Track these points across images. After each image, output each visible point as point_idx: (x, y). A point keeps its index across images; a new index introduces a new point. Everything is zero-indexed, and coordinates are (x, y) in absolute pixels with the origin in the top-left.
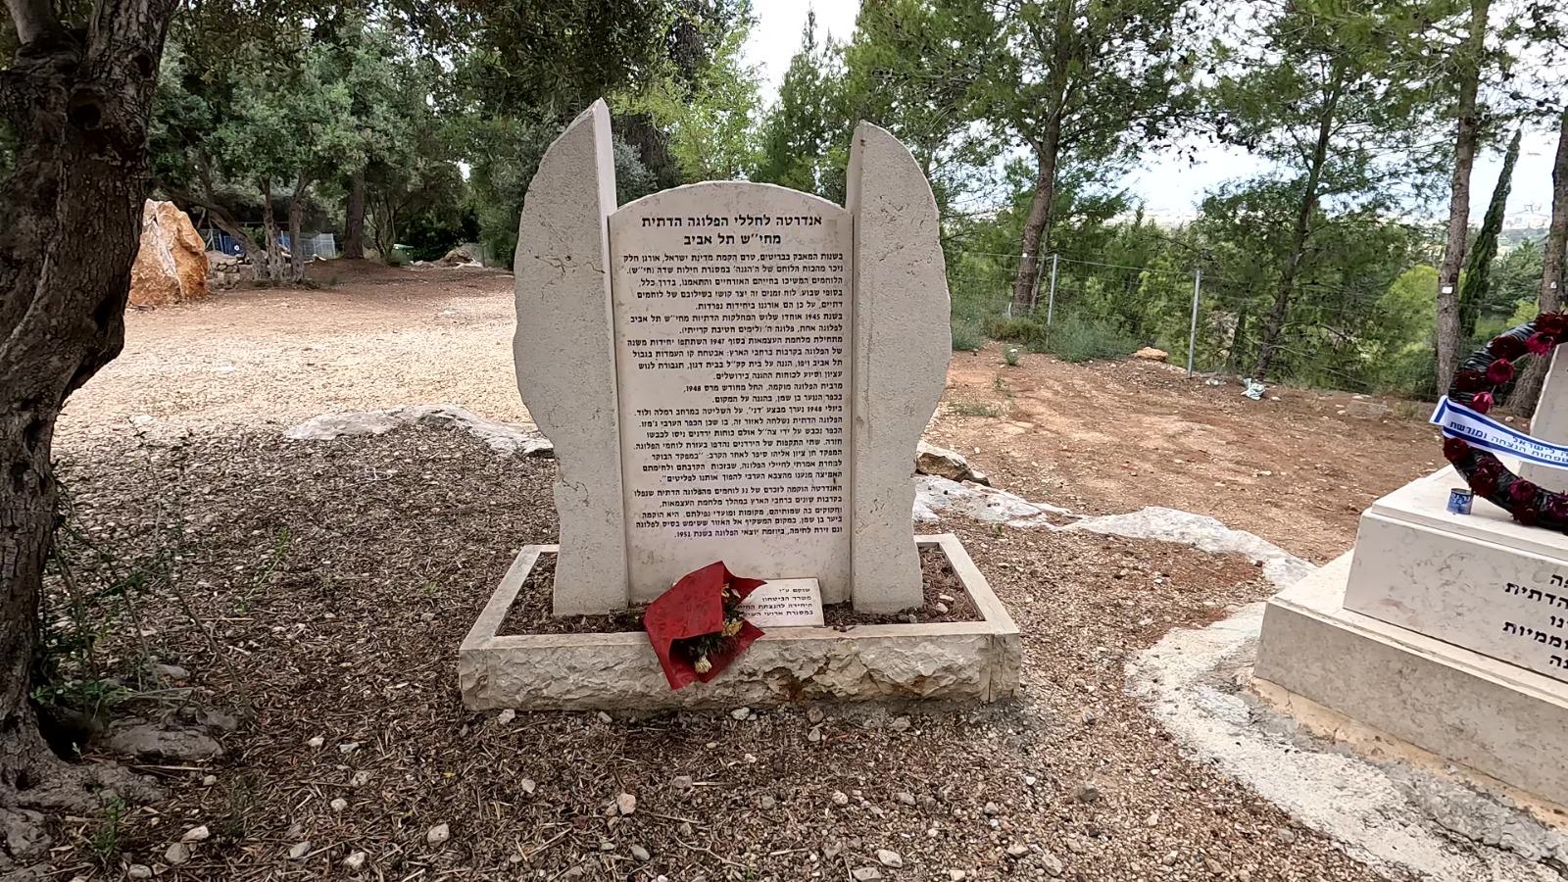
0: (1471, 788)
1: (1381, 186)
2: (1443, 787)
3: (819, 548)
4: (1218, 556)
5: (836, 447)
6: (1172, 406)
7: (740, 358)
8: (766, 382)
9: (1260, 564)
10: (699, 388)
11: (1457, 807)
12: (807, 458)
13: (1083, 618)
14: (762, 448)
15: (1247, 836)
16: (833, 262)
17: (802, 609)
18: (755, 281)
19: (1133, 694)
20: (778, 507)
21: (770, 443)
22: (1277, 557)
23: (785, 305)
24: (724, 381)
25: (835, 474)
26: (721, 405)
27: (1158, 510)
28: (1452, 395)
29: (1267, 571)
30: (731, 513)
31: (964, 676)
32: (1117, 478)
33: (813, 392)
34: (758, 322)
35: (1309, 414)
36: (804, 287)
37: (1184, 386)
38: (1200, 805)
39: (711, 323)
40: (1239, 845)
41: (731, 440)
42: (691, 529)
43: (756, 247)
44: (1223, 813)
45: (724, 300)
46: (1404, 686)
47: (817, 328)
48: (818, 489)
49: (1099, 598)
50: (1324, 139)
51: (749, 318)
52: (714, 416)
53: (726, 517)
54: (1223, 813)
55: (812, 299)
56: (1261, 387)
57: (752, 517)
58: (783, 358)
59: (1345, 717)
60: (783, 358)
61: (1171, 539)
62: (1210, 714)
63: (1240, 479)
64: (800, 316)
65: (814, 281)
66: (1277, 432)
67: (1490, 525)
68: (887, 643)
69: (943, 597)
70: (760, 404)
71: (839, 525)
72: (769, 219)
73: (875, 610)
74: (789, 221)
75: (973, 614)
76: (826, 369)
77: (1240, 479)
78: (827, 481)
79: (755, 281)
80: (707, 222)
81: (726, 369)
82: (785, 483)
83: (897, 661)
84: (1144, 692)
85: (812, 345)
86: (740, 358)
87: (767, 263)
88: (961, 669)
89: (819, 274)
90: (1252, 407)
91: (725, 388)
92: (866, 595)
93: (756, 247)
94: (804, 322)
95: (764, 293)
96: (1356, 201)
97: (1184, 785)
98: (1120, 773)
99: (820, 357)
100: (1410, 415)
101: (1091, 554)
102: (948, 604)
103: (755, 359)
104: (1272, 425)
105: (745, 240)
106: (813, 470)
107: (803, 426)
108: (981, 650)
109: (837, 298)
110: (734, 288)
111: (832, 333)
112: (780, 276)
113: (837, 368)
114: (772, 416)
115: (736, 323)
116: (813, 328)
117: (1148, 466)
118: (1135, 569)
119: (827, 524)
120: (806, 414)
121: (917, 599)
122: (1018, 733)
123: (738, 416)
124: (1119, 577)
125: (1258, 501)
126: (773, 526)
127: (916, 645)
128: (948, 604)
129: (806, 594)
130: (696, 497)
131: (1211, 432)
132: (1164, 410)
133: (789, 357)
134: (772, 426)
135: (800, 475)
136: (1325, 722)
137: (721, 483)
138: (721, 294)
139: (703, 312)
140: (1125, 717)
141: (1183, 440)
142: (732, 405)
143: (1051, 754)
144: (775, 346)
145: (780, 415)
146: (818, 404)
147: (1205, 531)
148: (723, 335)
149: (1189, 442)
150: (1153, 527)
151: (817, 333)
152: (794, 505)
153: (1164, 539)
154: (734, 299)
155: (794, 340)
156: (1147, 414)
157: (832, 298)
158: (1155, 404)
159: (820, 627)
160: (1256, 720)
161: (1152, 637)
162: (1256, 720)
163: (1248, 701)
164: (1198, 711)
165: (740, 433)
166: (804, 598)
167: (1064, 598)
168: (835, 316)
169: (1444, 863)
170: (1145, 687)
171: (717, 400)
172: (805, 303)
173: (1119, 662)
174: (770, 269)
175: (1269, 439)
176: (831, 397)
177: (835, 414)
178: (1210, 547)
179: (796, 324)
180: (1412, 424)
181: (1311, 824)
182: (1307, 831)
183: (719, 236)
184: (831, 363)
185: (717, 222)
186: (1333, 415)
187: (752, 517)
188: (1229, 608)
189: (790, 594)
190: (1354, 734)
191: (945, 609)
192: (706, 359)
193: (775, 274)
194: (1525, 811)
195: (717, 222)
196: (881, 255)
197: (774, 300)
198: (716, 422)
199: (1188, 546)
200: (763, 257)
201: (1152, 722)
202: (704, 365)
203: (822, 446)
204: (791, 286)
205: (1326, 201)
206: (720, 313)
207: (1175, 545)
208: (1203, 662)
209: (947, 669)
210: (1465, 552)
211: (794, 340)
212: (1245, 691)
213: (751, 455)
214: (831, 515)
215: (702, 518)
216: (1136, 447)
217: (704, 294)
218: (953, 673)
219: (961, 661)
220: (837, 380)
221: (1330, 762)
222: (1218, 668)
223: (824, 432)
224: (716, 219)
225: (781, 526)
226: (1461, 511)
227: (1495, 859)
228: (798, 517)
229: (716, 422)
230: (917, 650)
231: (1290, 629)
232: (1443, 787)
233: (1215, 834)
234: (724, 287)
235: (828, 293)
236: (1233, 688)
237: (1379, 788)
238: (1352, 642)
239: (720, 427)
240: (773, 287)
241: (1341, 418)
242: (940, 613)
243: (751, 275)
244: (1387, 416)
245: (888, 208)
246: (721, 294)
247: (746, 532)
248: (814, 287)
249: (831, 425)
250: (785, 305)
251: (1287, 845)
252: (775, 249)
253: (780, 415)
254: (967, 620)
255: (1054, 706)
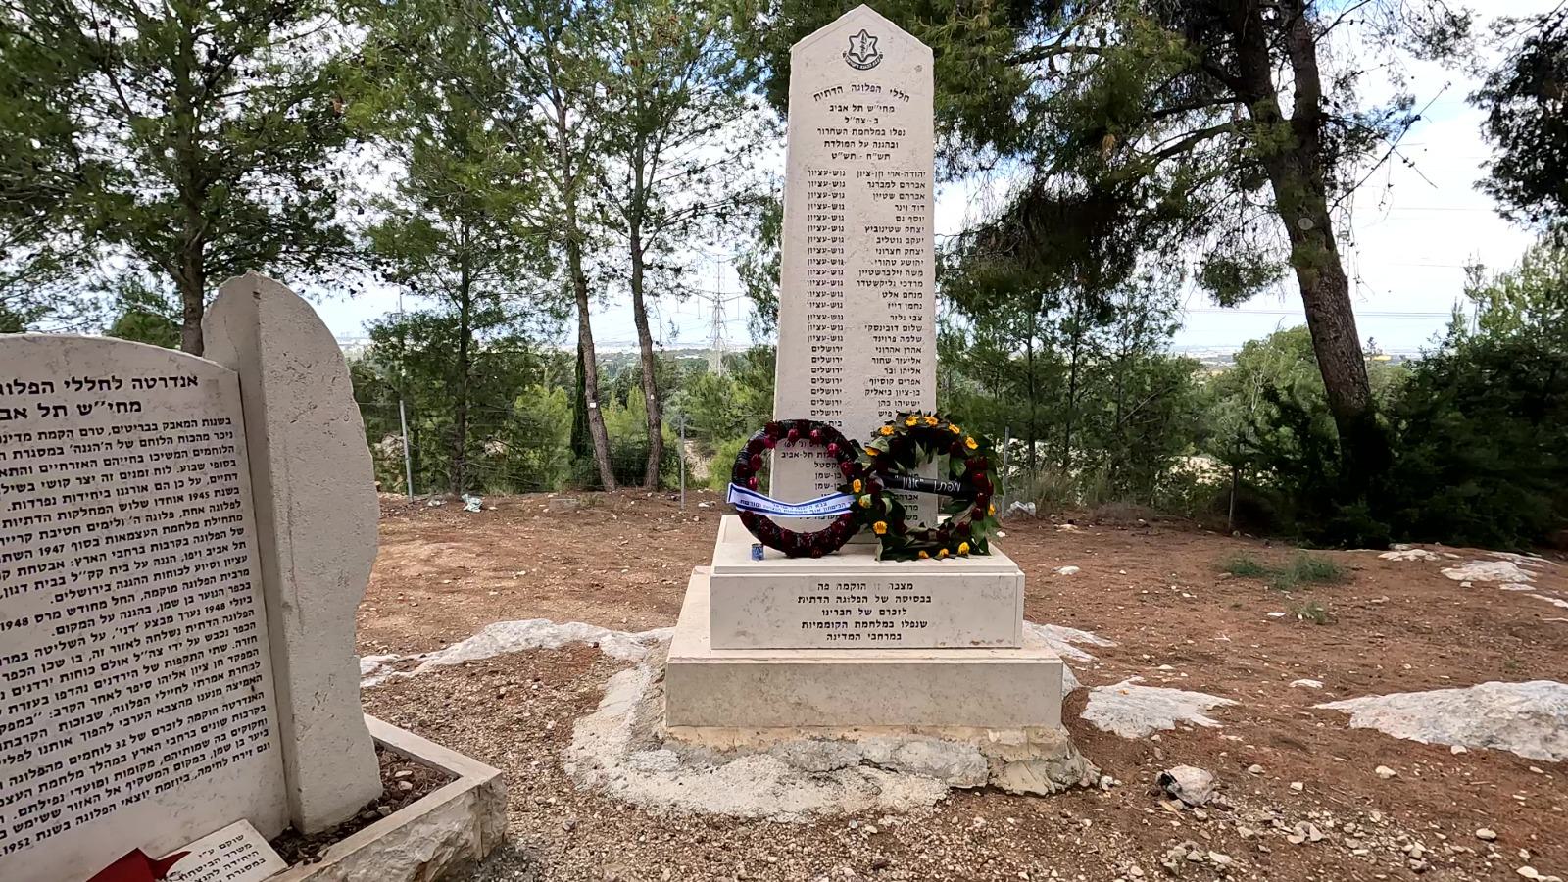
0: (815, 739)
1: (517, 324)
2: (802, 745)
3: (247, 778)
4: (563, 649)
5: (250, 647)
6: (409, 532)
7: (94, 566)
8: (138, 590)
9: (597, 645)
10: (26, 622)
11: (812, 755)
12: (212, 672)
13: (500, 745)
14: (143, 677)
15: (724, 847)
16: (219, 429)
17: (247, 862)
18: (107, 462)
19: (586, 787)
20: (176, 748)
21: (155, 668)
22: (605, 635)
23: (158, 486)
24: (70, 602)
25: (253, 680)
26: (66, 637)
27: (499, 625)
28: (734, 481)
29: (604, 649)
30: (100, 783)
31: (462, 842)
32: (400, 612)
33: (211, 588)
34: (118, 514)
35: (524, 517)
36: (183, 461)
37: (411, 510)
38: (685, 844)
39: (36, 527)
40: (724, 856)
41: (89, 681)
42: (29, 833)
43: (102, 417)
44: (701, 841)
45: (58, 492)
46: (765, 688)
47: (207, 509)
48: (232, 705)
49: (498, 722)
50: (466, 282)
51: (102, 510)
52: (56, 655)
53: (92, 792)
54: (701, 841)
55: (194, 475)
56: (478, 500)
57: (135, 777)
58: (161, 554)
59: (734, 729)
60: (161, 554)
61: (521, 648)
62: (650, 772)
63: (504, 584)
64: (181, 498)
65: (196, 452)
66: (506, 535)
67: (776, 563)
68: (376, 848)
69: (399, 774)
70: (132, 621)
71: (266, 740)
72: (120, 382)
73: (330, 822)
74: (151, 384)
75: (441, 777)
76: (225, 555)
77: (504, 584)
78: (244, 692)
79: (107, 462)
80: (15, 389)
81: (70, 584)
82: (184, 713)
83: (391, 862)
84: (593, 781)
85: (203, 531)
86: (94, 566)
87: (124, 436)
88: (459, 834)
89: (203, 444)
90: (477, 519)
91: (71, 612)
92: (319, 807)
93: (102, 417)
94: (187, 504)
95: (124, 476)
96: (501, 332)
97: (667, 836)
98: (621, 855)
99: (215, 543)
100: (592, 503)
101: (467, 690)
102: (408, 779)
103: (118, 562)
104: (502, 532)
105: (84, 410)
106: (221, 684)
107: (200, 634)
108: (471, 806)
109: (230, 470)
110: (71, 473)
111: (228, 512)
112: (146, 452)
113: (240, 553)
114: (152, 631)
115: (82, 521)
116: (202, 510)
117: (421, 593)
118: (509, 684)
119: (249, 745)
120: (204, 617)
121: (375, 787)
122: (524, 871)
123: (99, 645)
124: (501, 697)
125: (530, 599)
126: (172, 776)
127: (407, 834)
128: (408, 779)
129: (241, 844)
130: (34, 783)
131: (458, 548)
132: (406, 537)
133: (172, 550)
134: (154, 646)
135: (201, 698)
136: (724, 737)
137: (80, 746)
138: (51, 485)
139: (21, 513)
140: (593, 810)
141: (438, 561)
142: (86, 633)
143: (560, 872)
144: (147, 542)
145: (166, 628)
146: (219, 600)
147: (544, 632)
148: (61, 538)
149: (443, 561)
150: (501, 642)
151: (208, 515)
152: (201, 737)
153: (515, 649)
154: (75, 487)
155: (175, 529)
156: (391, 543)
157: (223, 471)
158: (393, 533)
159: (285, 871)
160: (684, 760)
161: (566, 736)
162: (684, 760)
163: (672, 748)
164: (642, 775)
165: (104, 667)
166: (241, 849)
167: (468, 735)
168: (229, 491)
169: (822, 795)
170: (592, 777)
171: (60, 631)
172: (186, 481)
173: (557, 768)
174: (130, 444)
175: (507, 544)
176: (236, 589)
177: (245, 607)
178: (554, 644)
179: (177, 508)
180: (596, 510)
181: (751, 815)
182: (751, 821)
183: (40, 407)
184: (231, 547)
185: (35, 389)
186: (541, 513)
187: (135, 777)
188: (599, 687)
189: (218, 853)
190: (744, 738)
191: (408, 785)
192: (30, 579)
193: (137, 450)
194: (843, 738)
195: (35, 389)
196: (292, 417)
197: (141, 482)
198: (60, 663)
199: (537, 649)
200: (116, 430)
201: (615, 802)
202: (31, 587)
203: (231, 651)
204: (163, 462)
205: (477, 335)
206: (52, 510)
207: (526, 651)
208: (619, 737)
209: (446, 843)
210: (773, 584)
211: (175, 529)
212: (668, 742)
213: (125, 692)
214: (252, 733)
215: (49, 808)
216: (400, 578)
217: (21, 488)
218: (450, 845)
219: (456, 827)
220: (242, 566)
221: (739, 764)
222: (635, 734)
223: (232, 632)
224: (32, 384)
225: (183, 771)
226: (760, 558)
227: (841, 776)
228: (207, 751)
229: (60, 663)
230: (411, 839)
231: (677, 681)
232: (802, 745)
233: (707, 858)
234: (54, 475)
235: (216, 465)
236: (658, 743)
237: (770, 766)
238: (727, 670)
239: (69, 667)
240: (137, 467)
241: (548, 515)
242: (407, 792)
243: (100, 455)
244: (578, 506)
245: (294, 364)
246: (51, 485)
247: (129, 800)
248: (197, 461)
249: (241, 622)
250: (158, 486)
251: (748, 837)
252: (133, 418)
253: (166, 628)
254: (439, 786)
255: (535, 830)
